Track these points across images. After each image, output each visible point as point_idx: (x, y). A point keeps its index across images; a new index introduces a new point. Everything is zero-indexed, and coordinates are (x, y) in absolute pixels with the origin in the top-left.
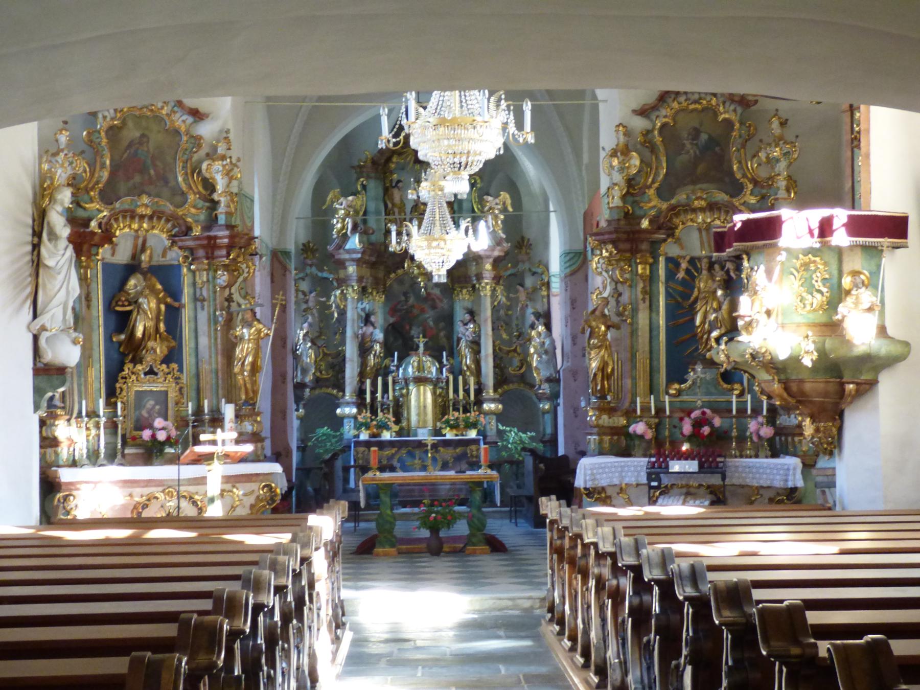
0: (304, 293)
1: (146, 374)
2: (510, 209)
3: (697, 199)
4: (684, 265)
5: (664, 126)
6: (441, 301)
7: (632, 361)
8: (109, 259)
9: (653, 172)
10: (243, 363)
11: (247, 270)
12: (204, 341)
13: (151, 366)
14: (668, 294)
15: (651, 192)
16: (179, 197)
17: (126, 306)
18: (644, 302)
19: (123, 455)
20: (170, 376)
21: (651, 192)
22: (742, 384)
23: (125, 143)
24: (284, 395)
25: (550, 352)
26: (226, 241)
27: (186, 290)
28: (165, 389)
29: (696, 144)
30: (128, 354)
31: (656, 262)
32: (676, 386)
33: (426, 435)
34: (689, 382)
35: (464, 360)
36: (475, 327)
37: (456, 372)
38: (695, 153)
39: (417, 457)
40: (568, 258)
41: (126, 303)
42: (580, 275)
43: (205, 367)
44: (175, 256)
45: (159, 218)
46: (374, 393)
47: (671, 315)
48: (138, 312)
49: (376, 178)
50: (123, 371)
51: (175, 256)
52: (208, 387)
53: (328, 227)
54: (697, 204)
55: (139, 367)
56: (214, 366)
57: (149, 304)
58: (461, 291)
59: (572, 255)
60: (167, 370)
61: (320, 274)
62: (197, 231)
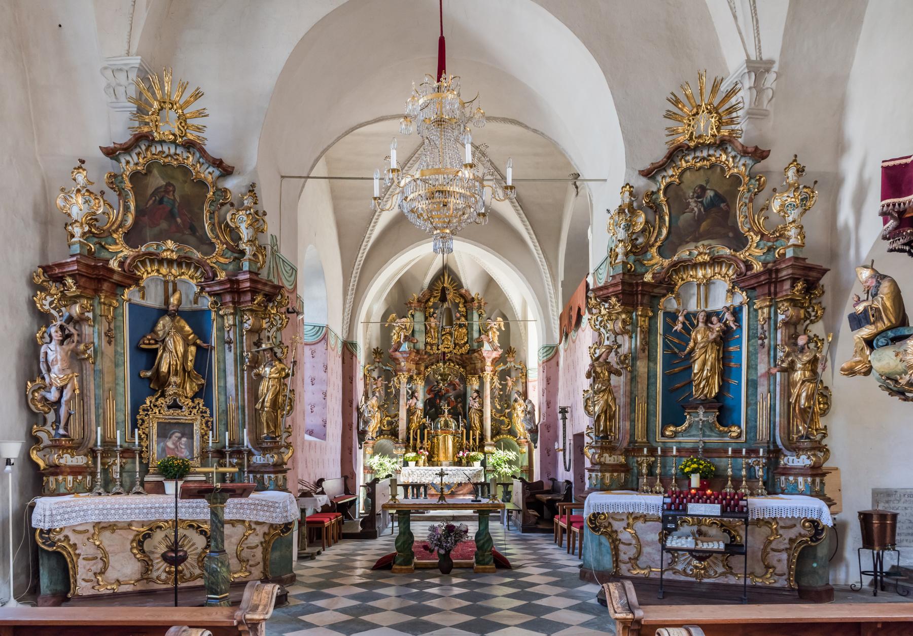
0: (374, 379)
1: (169, 407)
2: (503, 329)
3: (700, 254)
4: (681, 318)
5: (668, 186)
6: (459, 386)
7: (631, 405)
8: (137, 299)
9: (656, 232)
11: (280, 322)
12: (231, 380)
14: (666, 346)
15: (654, 250)
16: (207, 245)
18: (644, 351)
19: (142, 484)
21: (654, 250)
22: (739, 427)
23: (150, 191)
24: (351, 438)
25: (530, 413)
26: (248, 284)
29: (702, 202)
30: (158, 391)
31: (655, 316)
32: (672, 428)
34: (686, 424)
37: (469, 428)
38: (699, 210)
40: (545, 350)
41: (152, 342)
42: (553, 362)
44: (206, 302)
46: (415, 440)
47: (668, 363)
48: (164, 350)
49: (421, 311)
51: (206, 302)
53: (390, 338)
54: (700, 259)
55: (161, 400)
57: (176, 345)
59: (548, 348)
61: (384, 368)
62: (222, 276)
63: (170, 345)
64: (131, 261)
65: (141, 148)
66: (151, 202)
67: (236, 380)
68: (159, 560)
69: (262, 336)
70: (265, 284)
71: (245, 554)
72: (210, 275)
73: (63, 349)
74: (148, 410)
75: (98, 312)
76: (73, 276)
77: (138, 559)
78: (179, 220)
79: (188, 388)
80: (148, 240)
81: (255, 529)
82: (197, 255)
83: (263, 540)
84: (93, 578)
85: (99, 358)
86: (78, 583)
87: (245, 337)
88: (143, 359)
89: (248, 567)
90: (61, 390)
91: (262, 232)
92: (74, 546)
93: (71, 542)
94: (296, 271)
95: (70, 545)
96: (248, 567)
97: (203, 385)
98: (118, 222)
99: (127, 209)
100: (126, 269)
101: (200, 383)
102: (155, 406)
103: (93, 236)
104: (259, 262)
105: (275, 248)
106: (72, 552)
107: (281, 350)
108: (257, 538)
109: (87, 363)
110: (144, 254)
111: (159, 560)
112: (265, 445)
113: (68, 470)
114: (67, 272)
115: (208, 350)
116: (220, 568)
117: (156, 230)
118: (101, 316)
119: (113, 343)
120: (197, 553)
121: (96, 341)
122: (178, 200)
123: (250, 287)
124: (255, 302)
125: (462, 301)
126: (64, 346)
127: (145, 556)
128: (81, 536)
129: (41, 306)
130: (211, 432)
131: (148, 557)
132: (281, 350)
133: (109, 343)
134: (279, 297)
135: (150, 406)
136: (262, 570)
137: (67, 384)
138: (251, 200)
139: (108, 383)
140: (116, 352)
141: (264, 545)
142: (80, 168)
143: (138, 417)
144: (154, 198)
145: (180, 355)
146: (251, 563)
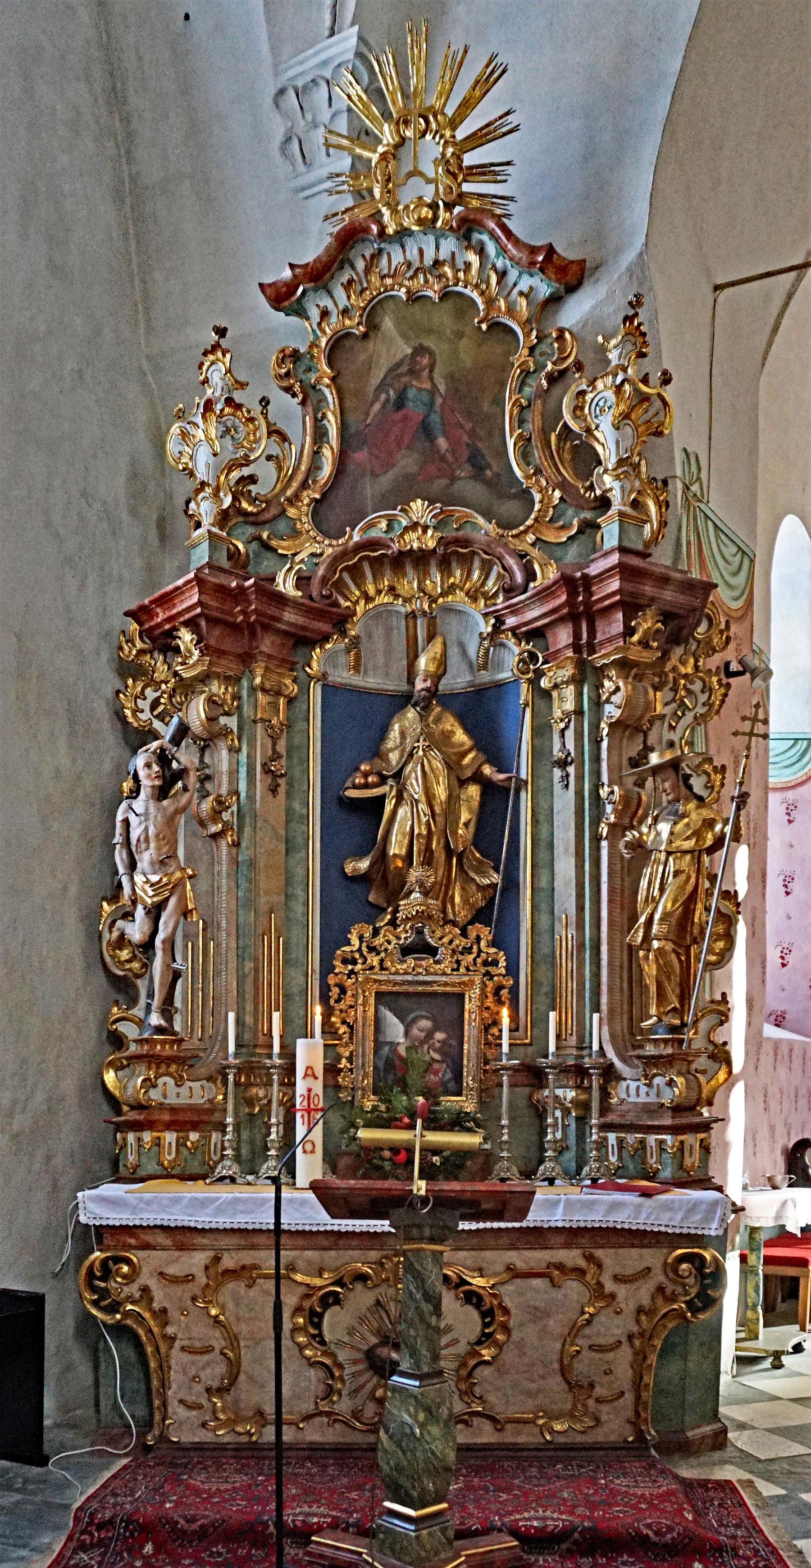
1: (406, 951)
8: (343, 676)
11: (703, 698)
23: (377, 376)
26: (615, 584)
30: (384, 910)
50: (348, 943)
60: (460, 942)
63: (415, 787)
64: (327, 570)
65: (353, 267)
66: (377, 407)
67: (580, 867)
68: (360, 1367)
69: (652, 740)
70: (663, 580)
71: (583, 1367)
72: (519, 578)
76: (191, 625)
77: (308, 1359)
79: (457, 899)
80: (370, 508)
81: (613, 1296)
83: (635, 1329)
84: (204, 1402)
86: (170, 1409)
87: (605, 744)
89: (591, 1402)
90: (155, 912)
91: (659, 434)
92: (162, 1315)
93: (156, 1305)
94: (752, 561)
95: (154, 1313)
96: (591, 1402)
98: (300, 477)
99: (320, 435)
100: (315, 594)
101: (486, 882)
102: (372, 949)
104: (649, 520)
105: (695, 488)
106: (156, 1330)
107: (704, 779)
108: (618, 1321)
111: (360, 1367)
112: (650, 1050)
113: (166, 1117)
114: (180, 614)
115: (508, 790)
116: (422, 1426)
120: (458, 1356)
122: (442, 388)
123: (619, 592)
124: (635, 638)
126: (165, 803)
127: (324, 1353)
128: (177, 1290)
129: (134, 712)
130: (505, 1012)
131: (332, 1355)
132: (704, 779)
134: (702, 628)
135: (360, 950)
136: (630, 1414)
137: (167, 899)
138: (629, 347)
139: (267, 892)
140: (289, 813)
141: (637, 1342)
142: (215, 347)
143: (331, 980)
144: (383, 397)
145: (437, 809)
146: (599, 1391)
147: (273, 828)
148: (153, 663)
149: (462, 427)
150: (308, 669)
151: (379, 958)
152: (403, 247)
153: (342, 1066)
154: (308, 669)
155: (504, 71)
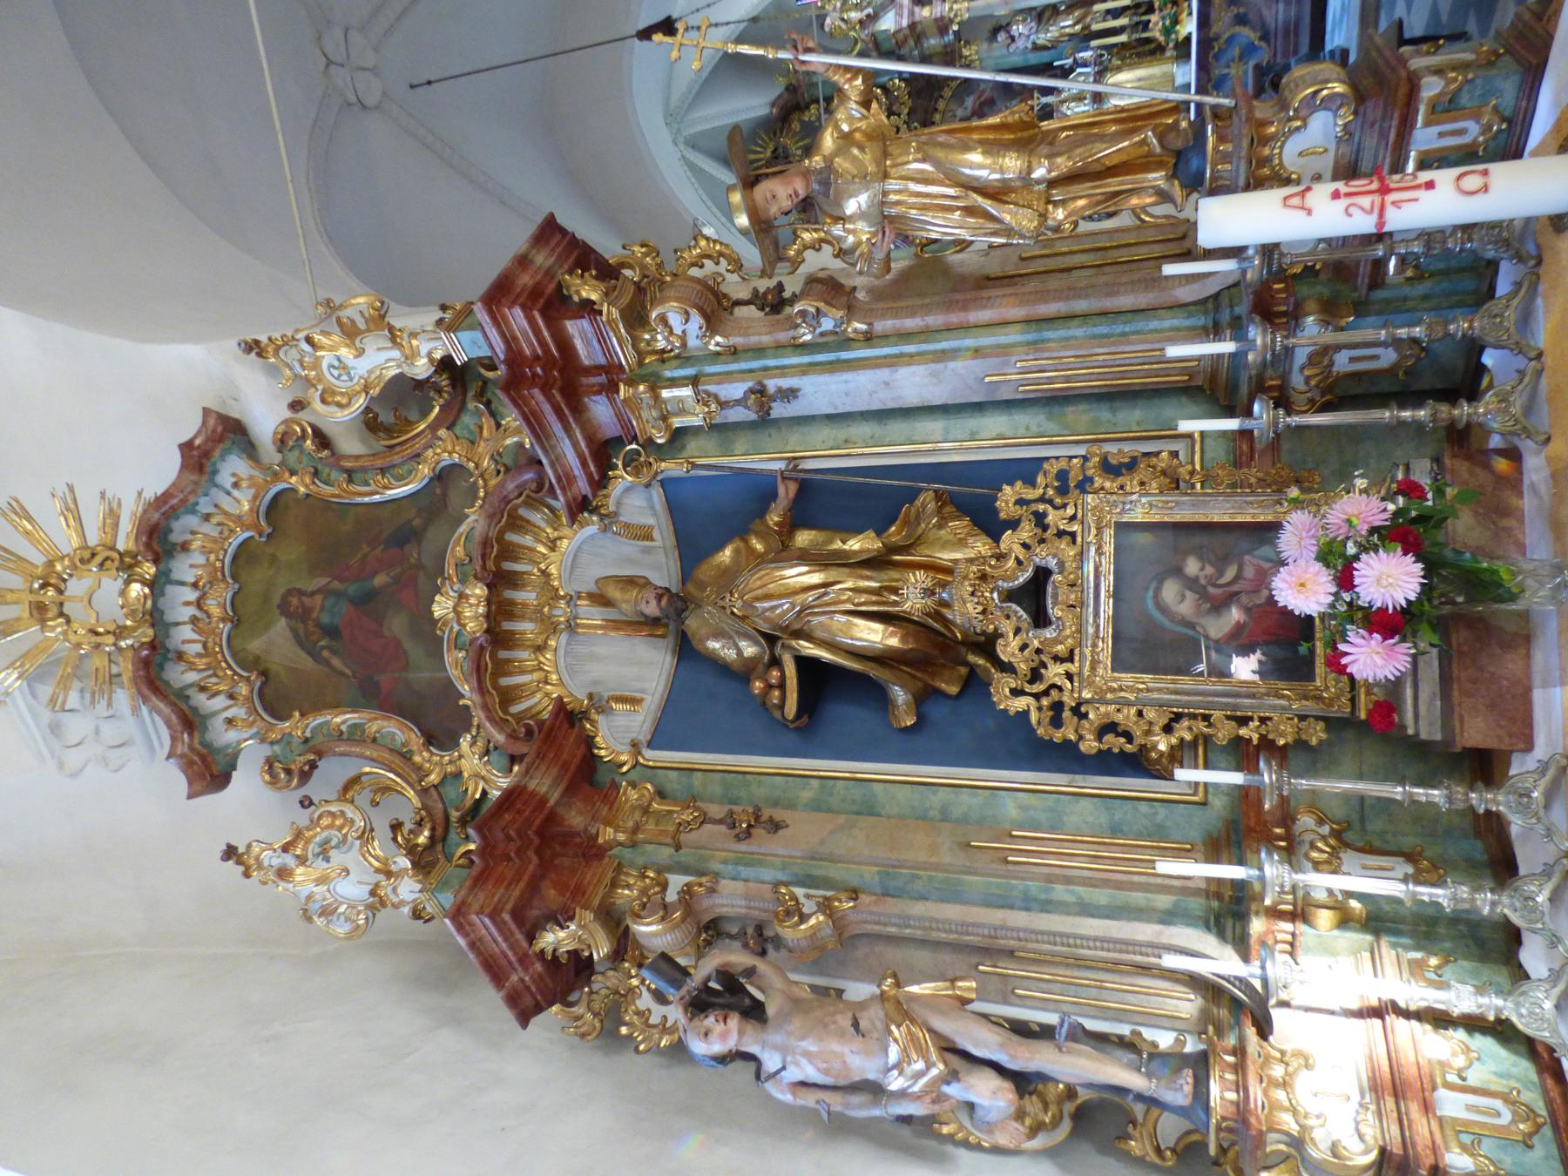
1: (1040, 619)
10: (997, 193)
13: (1011, 596)
17: (783, 677)
20: (1052, 517)
23: (306, 662)
26: (517, 318)
27: (1374, 416)
28: (1109, 535)
30: (973, 669)
33: (1187, 68)
35: (1067, 30)
36: (1017, 22)
39: (1226, 71)
43: (1015, 375)
45: (509, 552)
48: (799, 634)
52: (1101, 353)
55: (1008, 649)
56: (1012, 336)
58: (966, 57)
60: (1026, 532)
66: (336, 662)
67: (910, 359)
73: (784, 1016)
74: (1058, 707)
75: (665, 854)
78: (380, 580)
80: (443, 674)
82: (474, 520)
85: (836, 872)
88: (844, 714)
97: (938, 495)
99: (355, 736)
102: (1035, 676)
103: (444, 839)
107: (808, 254)
109: (853, 917)
110: (482, 690)
117: (414, 650)
118: (678, 847)
119: (779, 814)
121: (769, 875)
122: (322, 581)
125: (795, 116)
126: (771, 1010)
133: (776, 826)
135: (1037, 696)
140: (817, 806)
143: (1090, 745)
144: (325, 653)
145: (816, 578)
147: (832, 832)
148: (604, 992)
149: (366, 555)
150: (625, 769)
151: (1050, 663)
152: (177, 624)
153: (1255, 737)
154: (625, 769)
155: (17, 501)
